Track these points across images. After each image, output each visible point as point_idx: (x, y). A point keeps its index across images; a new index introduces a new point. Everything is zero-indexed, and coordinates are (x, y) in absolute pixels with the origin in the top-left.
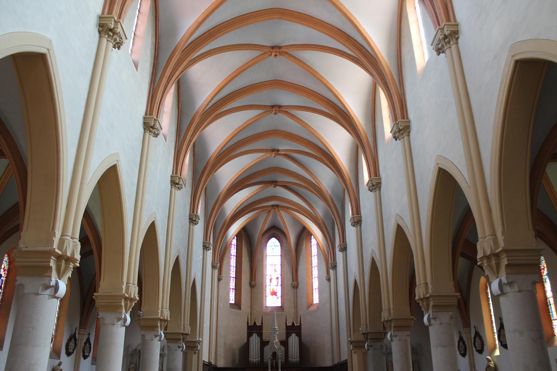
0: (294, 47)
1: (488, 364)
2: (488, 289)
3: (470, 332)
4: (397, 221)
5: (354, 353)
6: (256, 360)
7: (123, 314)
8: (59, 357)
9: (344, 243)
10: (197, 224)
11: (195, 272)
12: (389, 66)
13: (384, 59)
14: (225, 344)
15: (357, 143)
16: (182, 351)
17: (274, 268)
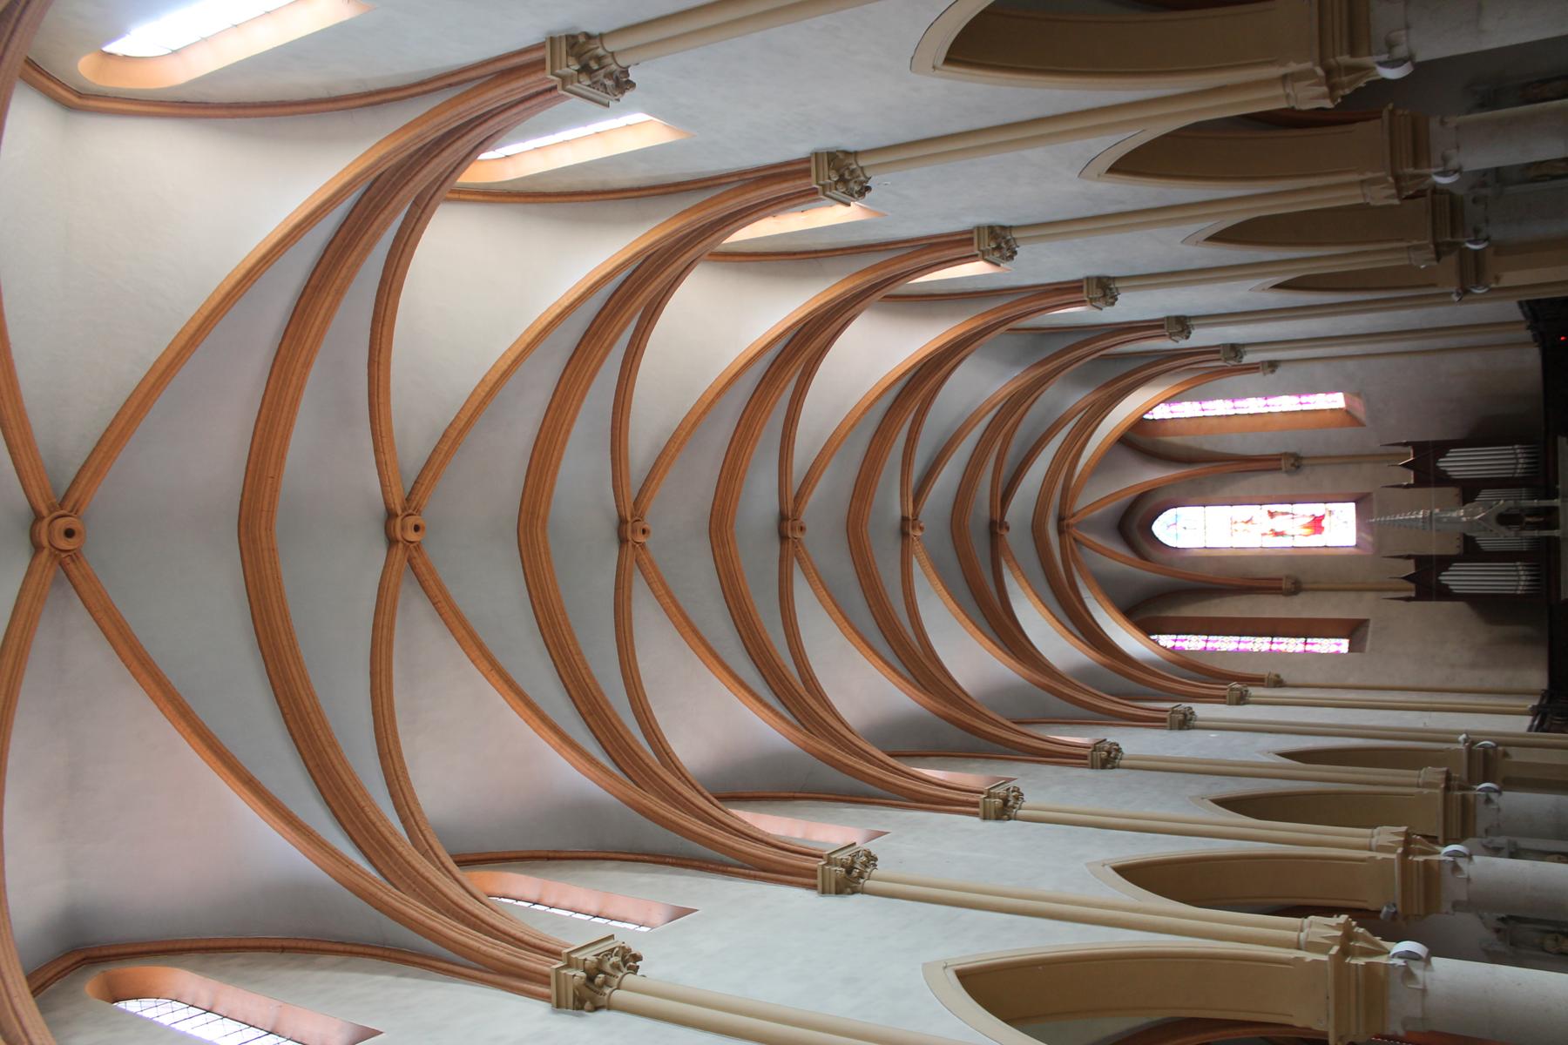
7: (1391, 962)
14: (1473, 666)
15: (879, 298)
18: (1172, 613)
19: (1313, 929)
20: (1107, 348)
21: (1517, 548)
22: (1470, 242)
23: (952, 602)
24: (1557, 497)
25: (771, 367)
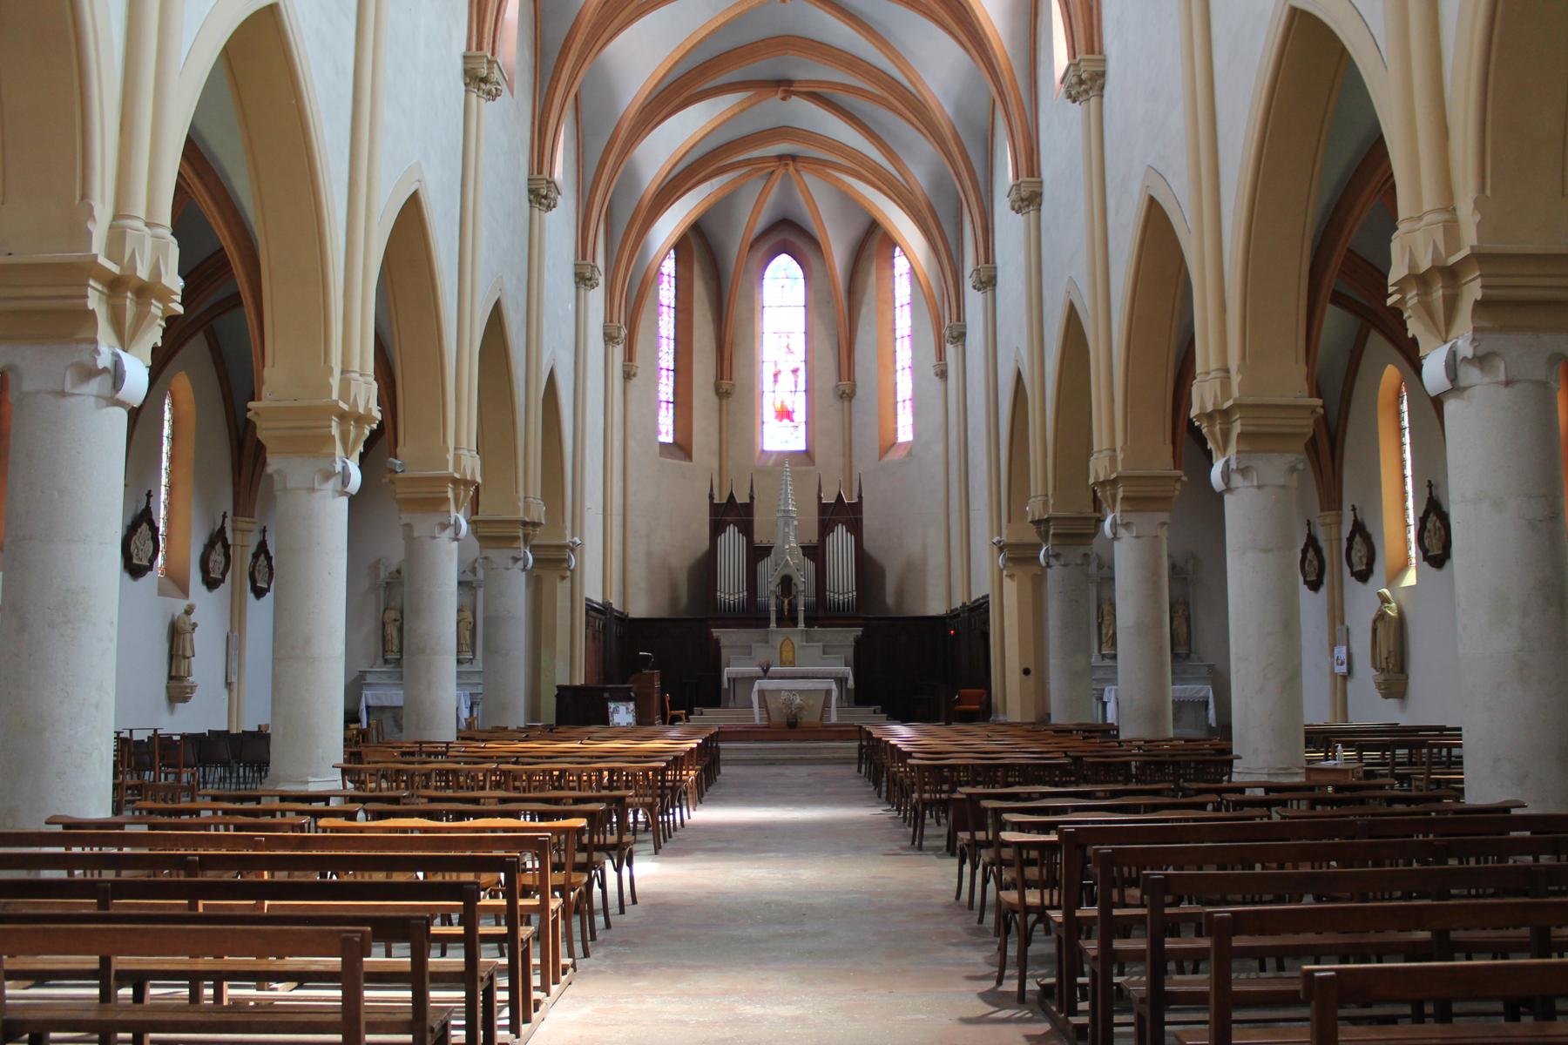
1: (1380, 610)
2: (1402, 403)
3: (1339, 523)
5: (1007, 576)
6: (737, 597)
7: (337, 459)
8: (185, 592)
9: (987, 265)
10: (554, 207)
14: (649, 554)
16: (524, 569)
17: (784, 341)
21: (759, 593)
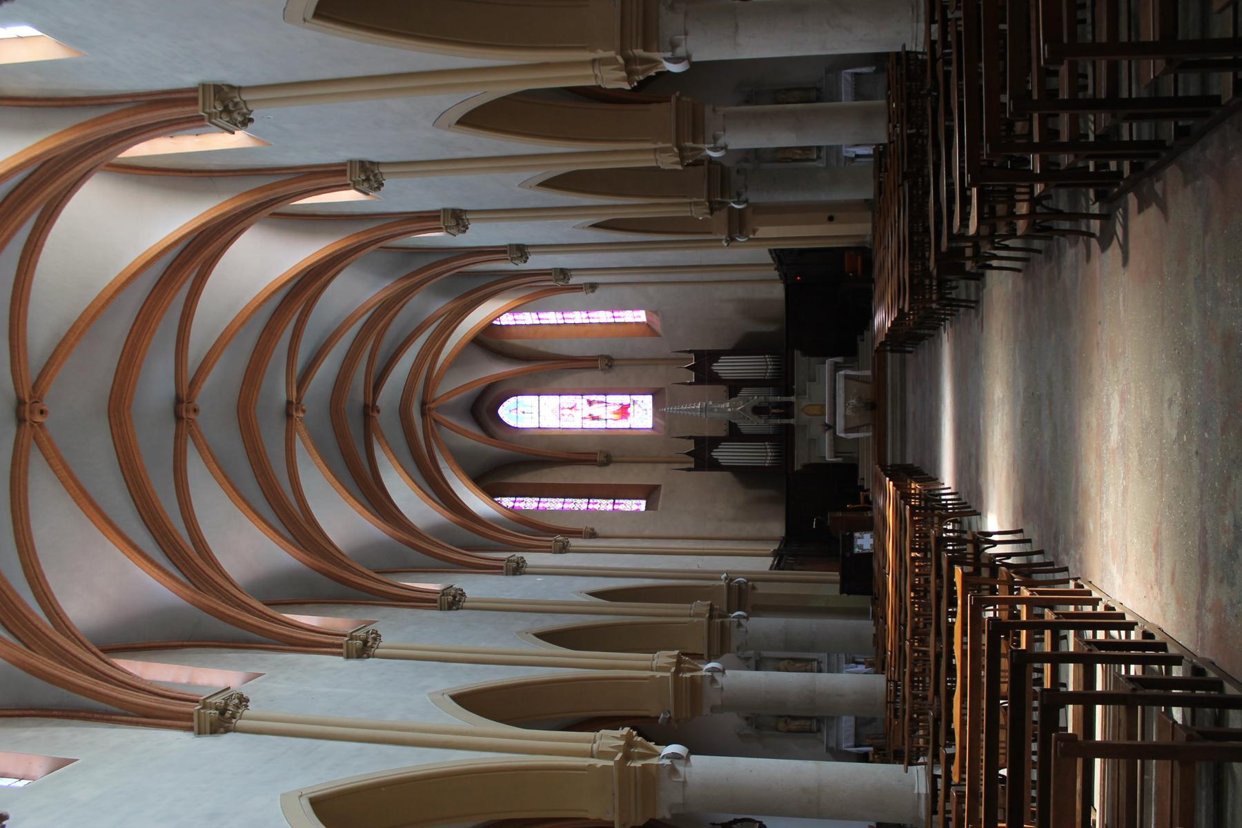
0: (18, 368)
4: (449, 126)
5: (754, 235)
6: (769, 450)
7: (661, 763)
9: (508, 252)
10: (462, 590)
11: (572, 593)
12: (60, 130)
13: (40, 142)
14: (734, 520)
15: (266, 215)
16: (747, 618)
17: (567, 412)
18: (512, 480)
19: (603, 741)
20: (462, 266)
22: (734, 202)
23: (329, 473)
24: (793, 395)
25: (168, 268)
